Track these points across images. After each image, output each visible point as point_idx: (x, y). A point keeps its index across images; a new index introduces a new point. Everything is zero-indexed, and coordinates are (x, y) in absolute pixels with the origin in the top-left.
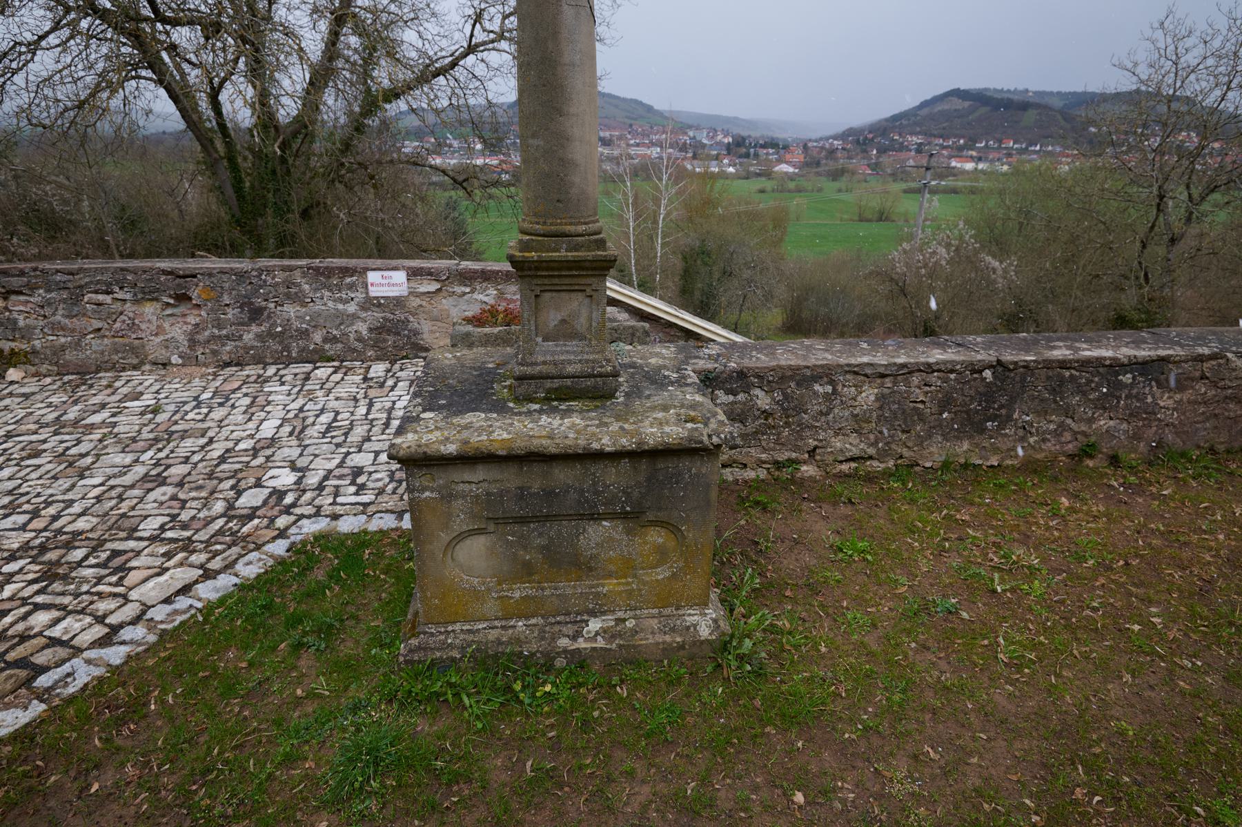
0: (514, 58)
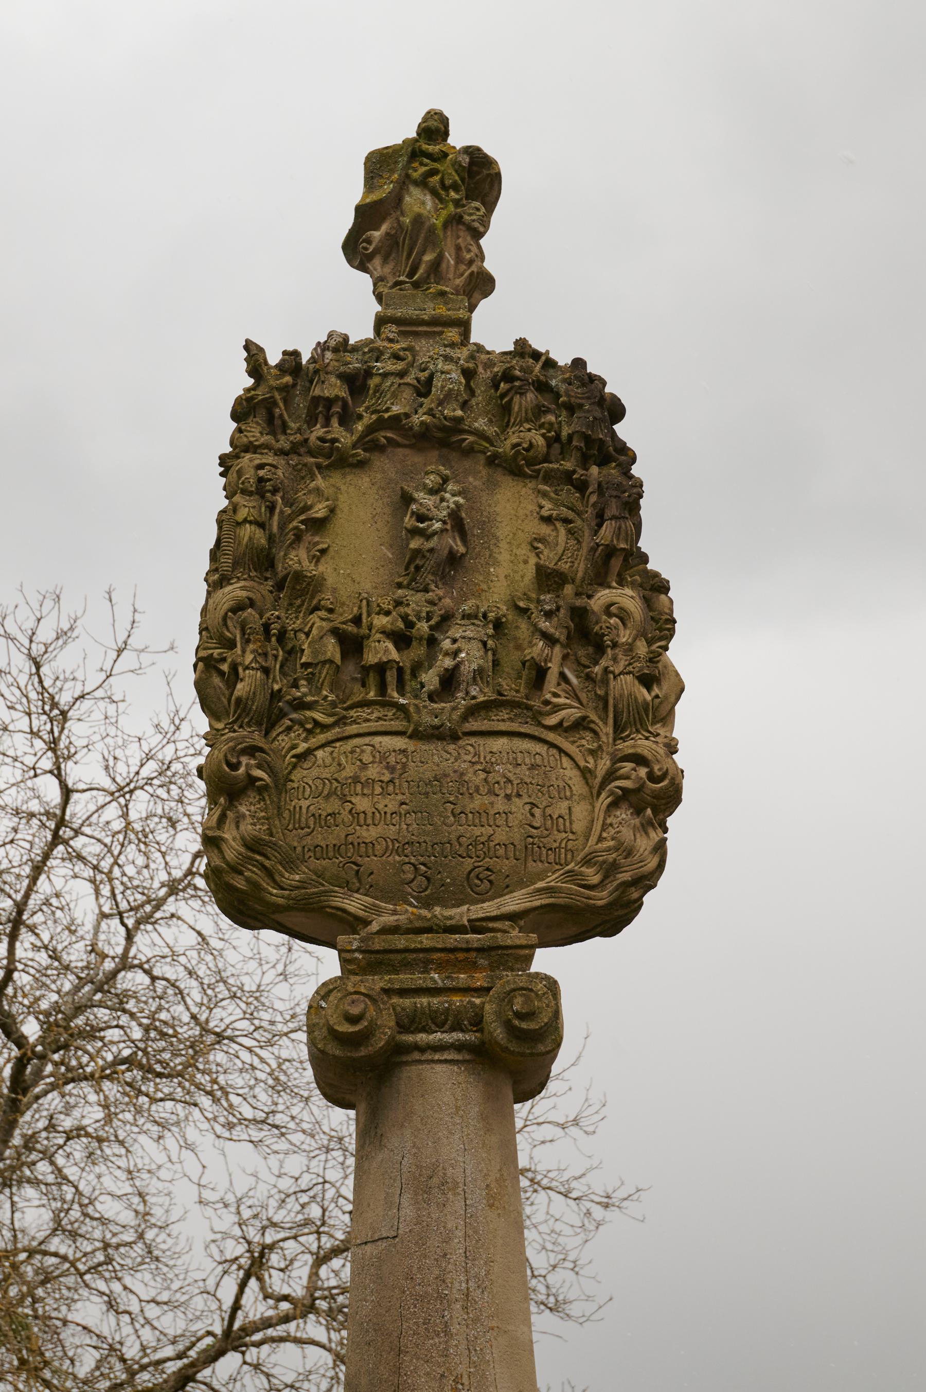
0: (339, 1358)
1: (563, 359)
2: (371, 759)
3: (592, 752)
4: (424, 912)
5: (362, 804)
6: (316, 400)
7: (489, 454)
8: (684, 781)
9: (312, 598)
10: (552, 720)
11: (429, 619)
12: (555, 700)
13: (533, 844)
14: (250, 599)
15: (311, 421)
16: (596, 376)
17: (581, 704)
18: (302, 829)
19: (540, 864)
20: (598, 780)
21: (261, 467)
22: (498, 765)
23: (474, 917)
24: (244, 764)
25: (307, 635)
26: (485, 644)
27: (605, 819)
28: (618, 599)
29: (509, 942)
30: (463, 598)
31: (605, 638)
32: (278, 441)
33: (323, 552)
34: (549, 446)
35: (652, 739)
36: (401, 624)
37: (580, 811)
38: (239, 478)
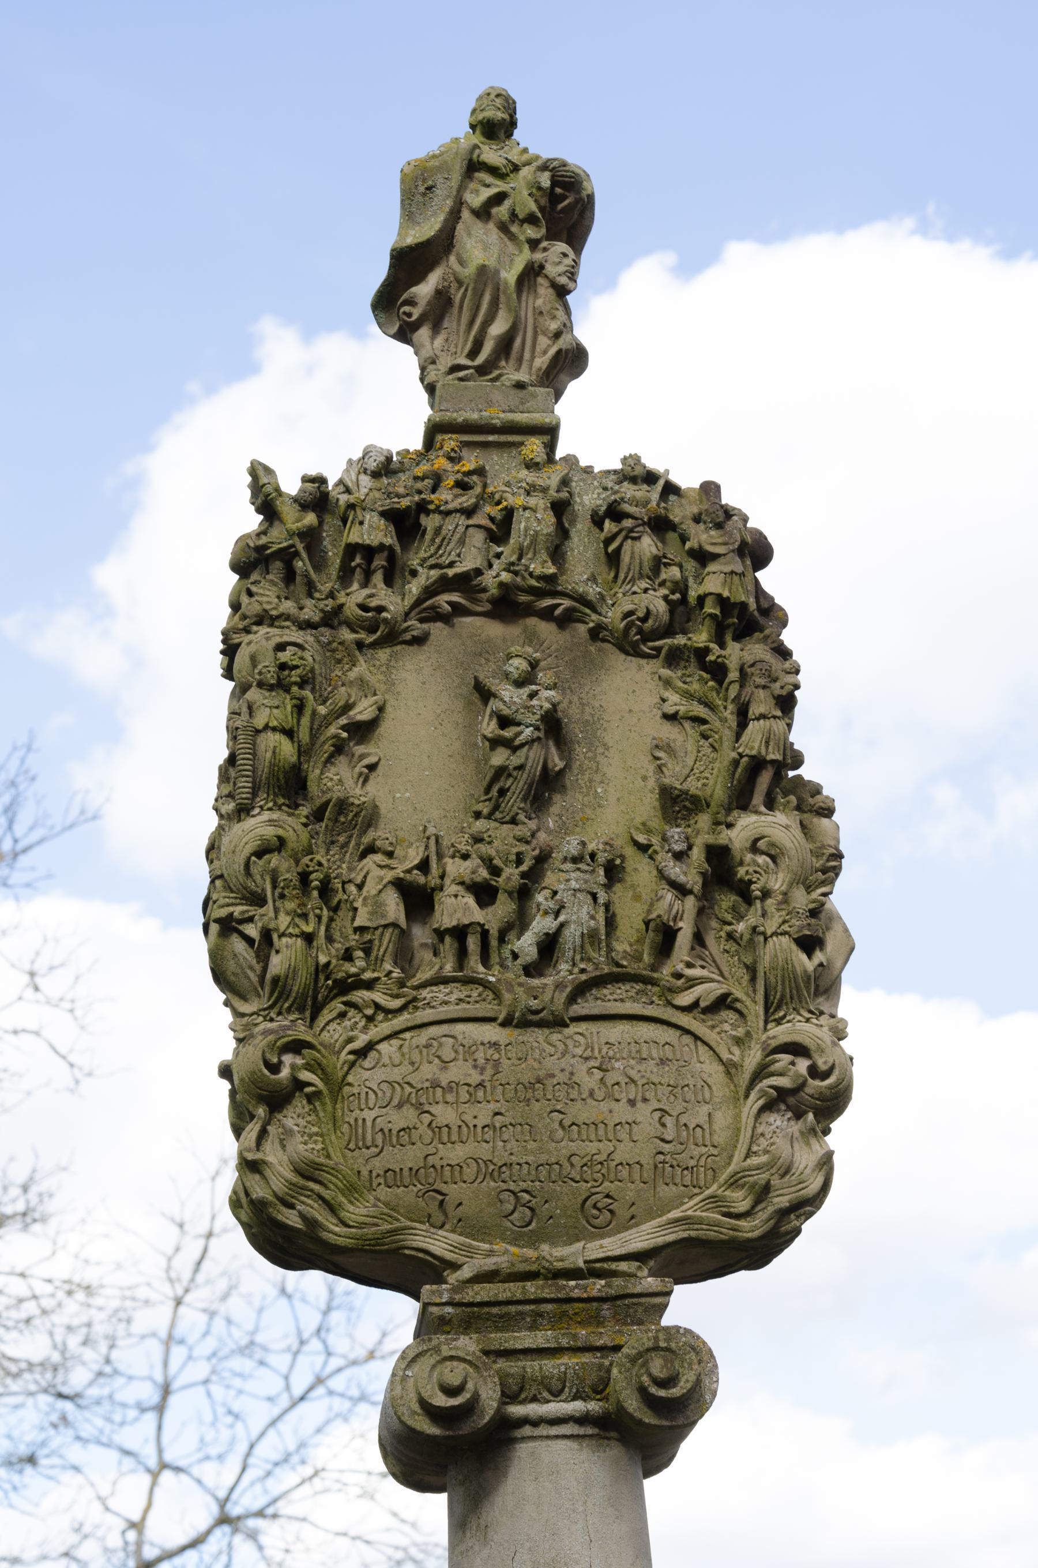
1: (687, 479)
2: (453, 1055)
3: (738, 1041)
4: (530, 1253)
5: (445, 1114)
6: (352, 550)
7: (591, 625)
8: (854, 1069)
9: (364, 832)
10: (685, 999)
11: (519, 862)
12: (689, 972)
13: (664, 1162)
14: (280, 838)
15: (346, 575)
16: (734, 509)
17: (722, 975)
18: (368, 1148)
19: (674, 1188)
20: (747, 1076)
21: (281, 647)
22: (617, 1060)
23: (593, 1257)
24: (287, 1064)
25: (360, 887)
26: (594, 897)
27: (754, 1127)
28: (767, 831)
29: (638, 1290)
30: (564, 830)
31: (753, 887)
32: (301, 608)
33: (372, 767)
34: (672, 612)
35: (814, 1021)
36: (484, 873)
37: (722, 1119)
38: (254, 666)
